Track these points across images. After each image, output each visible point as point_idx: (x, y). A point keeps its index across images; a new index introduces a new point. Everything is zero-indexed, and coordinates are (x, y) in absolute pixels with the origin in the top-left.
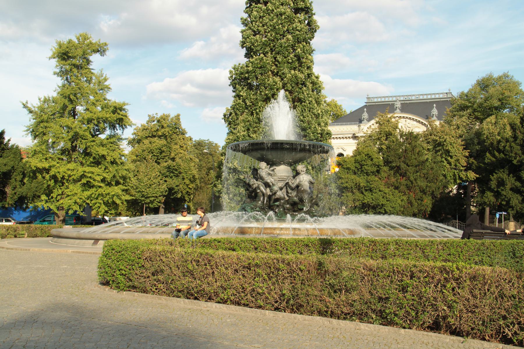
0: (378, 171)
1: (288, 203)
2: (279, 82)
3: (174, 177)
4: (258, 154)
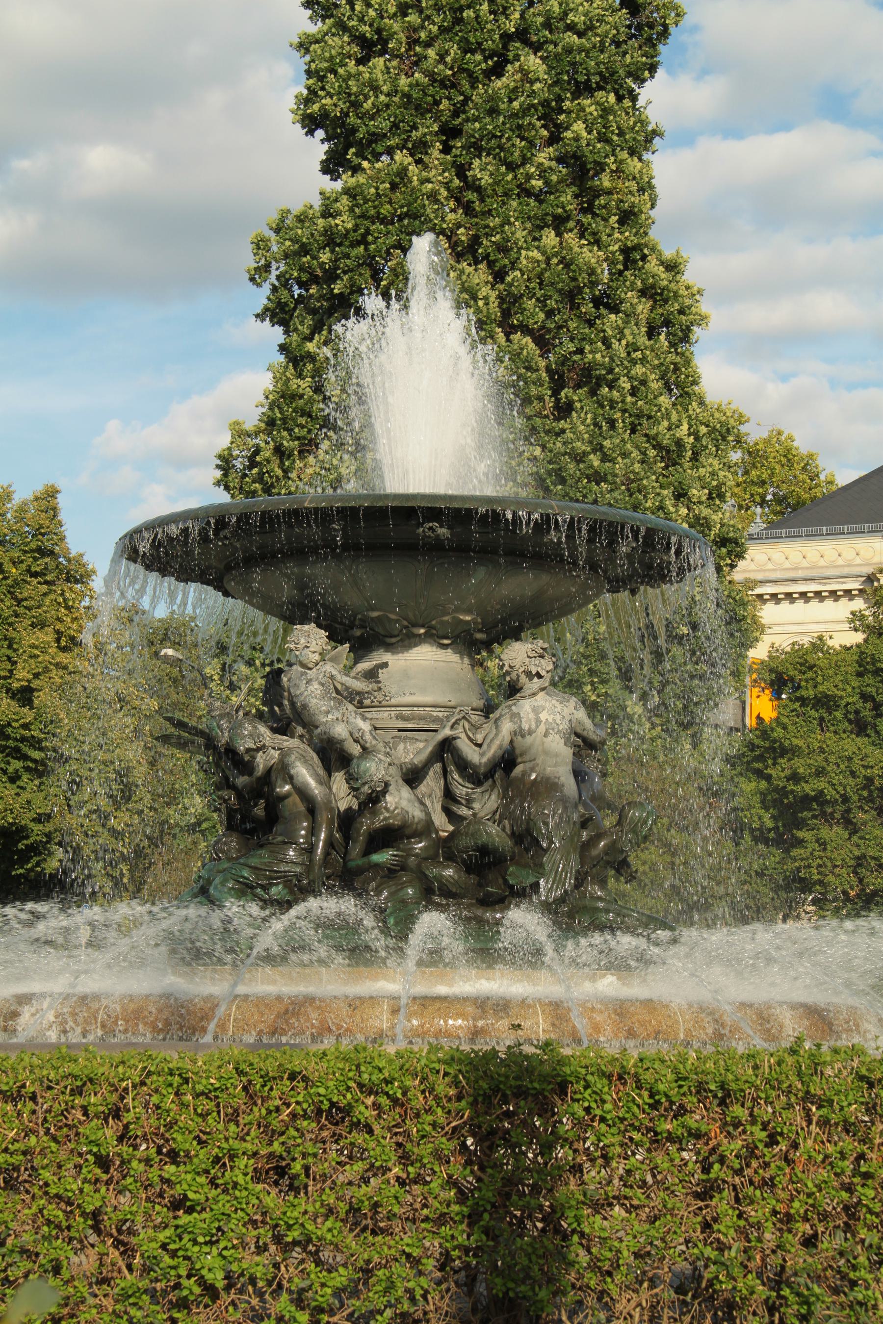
1: (450, 858)
2: (484, 291)
3: (25, 777)
4: (283, 583)
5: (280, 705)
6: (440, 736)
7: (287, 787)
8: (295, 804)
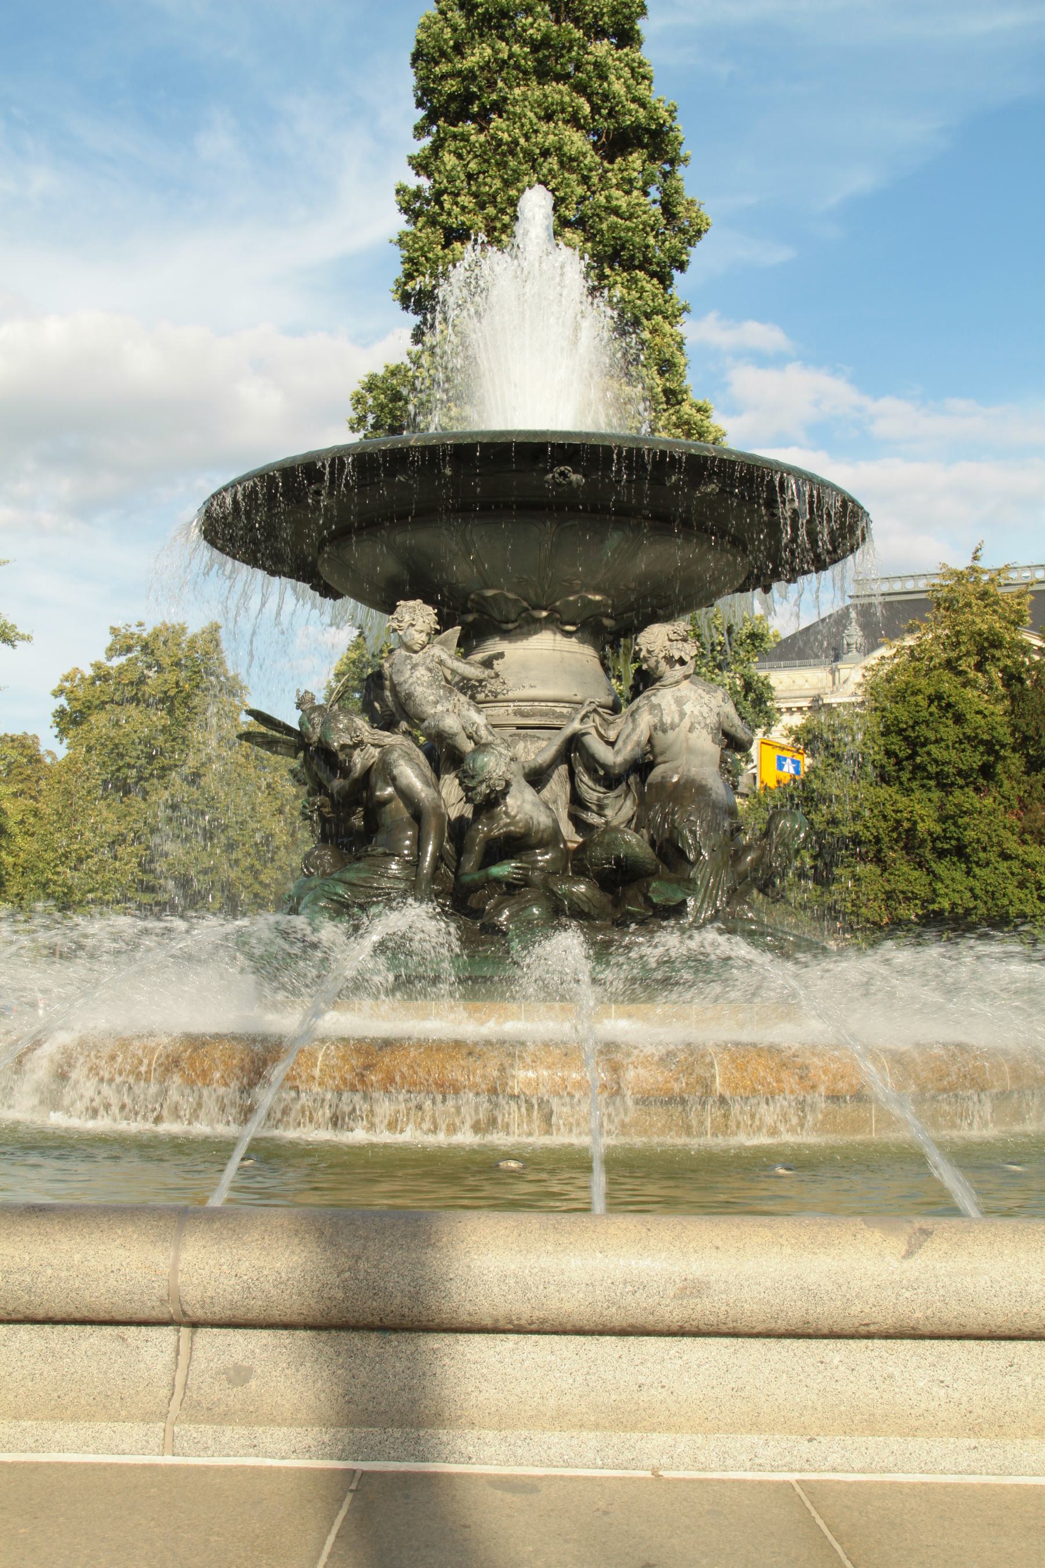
0: (987, 771)
1: (581, 873)
5: (382, 700)
6: (568, 731)
7: (390, 790)
8: (397, 809)
